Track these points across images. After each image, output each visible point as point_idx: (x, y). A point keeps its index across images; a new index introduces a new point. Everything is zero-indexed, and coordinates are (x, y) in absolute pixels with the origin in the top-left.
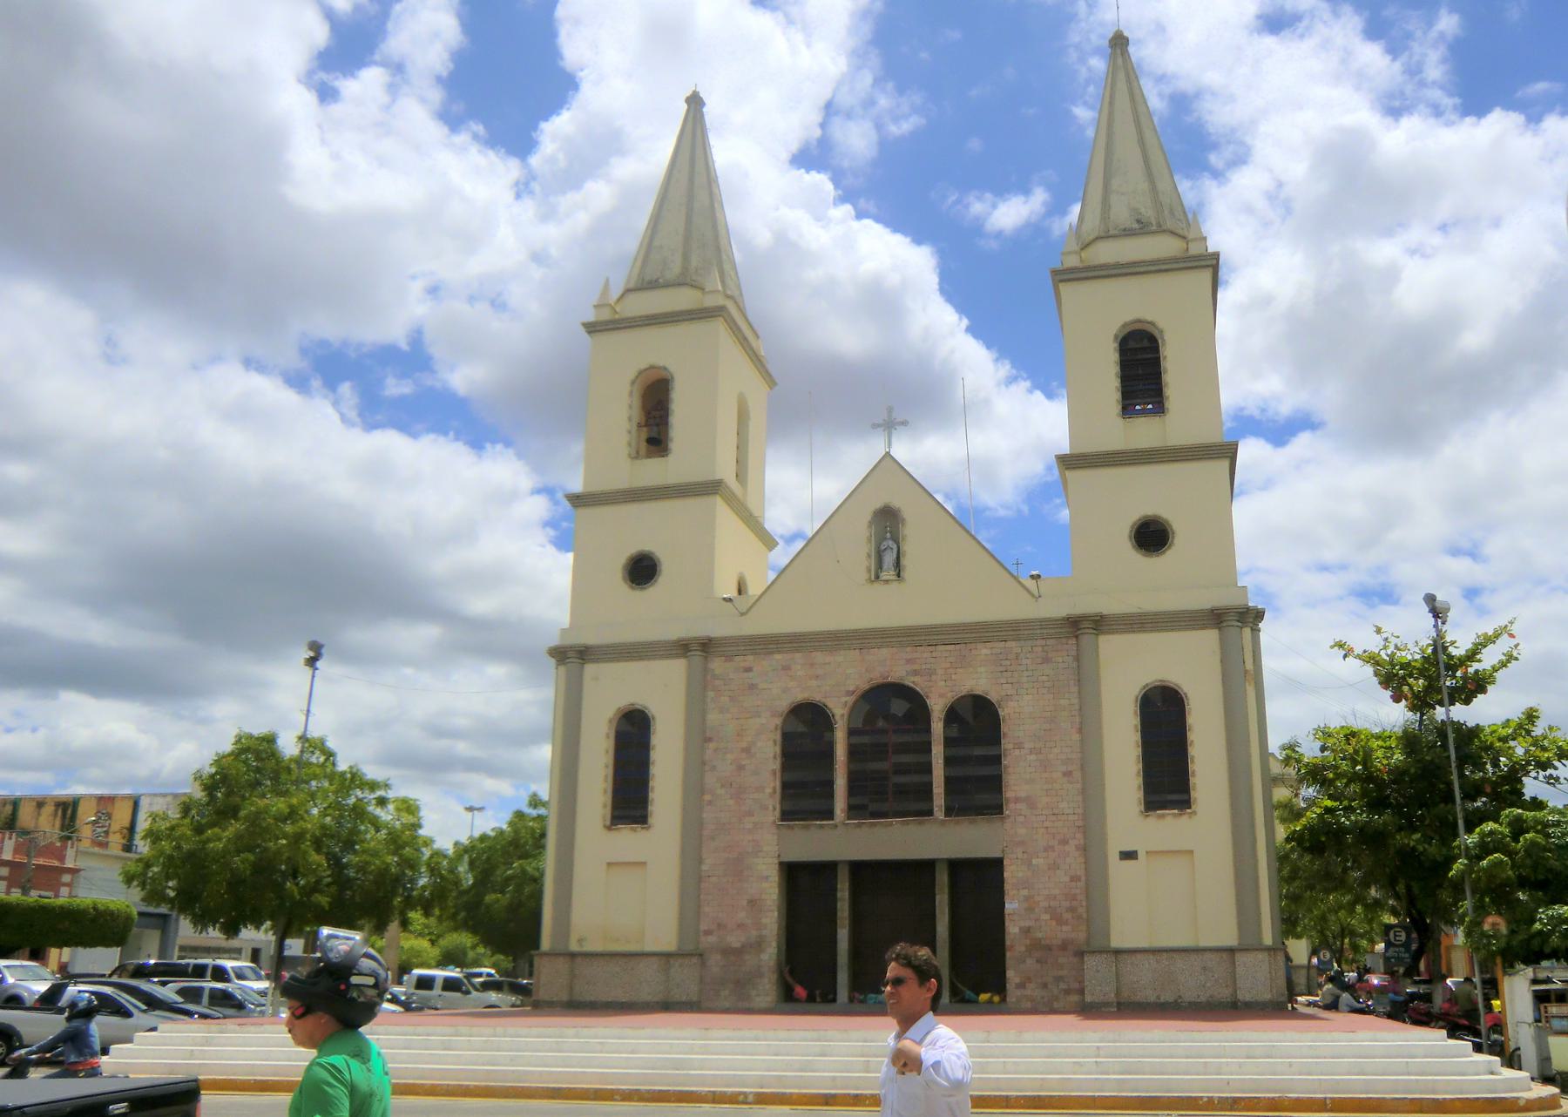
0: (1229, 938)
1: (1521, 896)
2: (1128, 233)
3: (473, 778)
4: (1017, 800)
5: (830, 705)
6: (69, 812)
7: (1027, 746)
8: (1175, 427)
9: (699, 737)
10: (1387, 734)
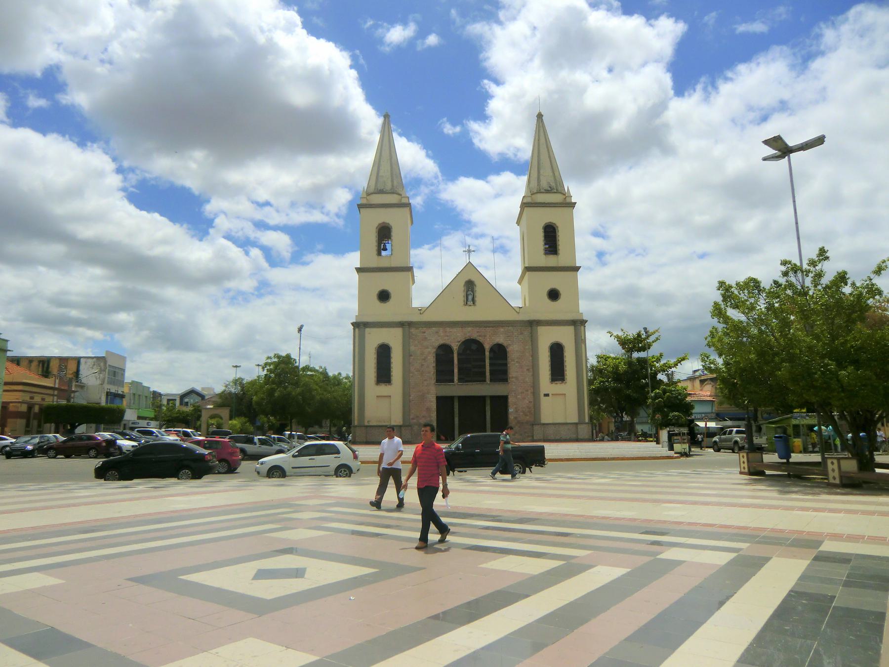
0: (576, 421)
1: (666, 410)
2: (547, 192)
3: (81, 330)
4: (512, 377)
5: (452, 345)
6: (46, 365)
7: (516, 361)
8: (561, 260)
9: (407, 356)
10: (617, 358)
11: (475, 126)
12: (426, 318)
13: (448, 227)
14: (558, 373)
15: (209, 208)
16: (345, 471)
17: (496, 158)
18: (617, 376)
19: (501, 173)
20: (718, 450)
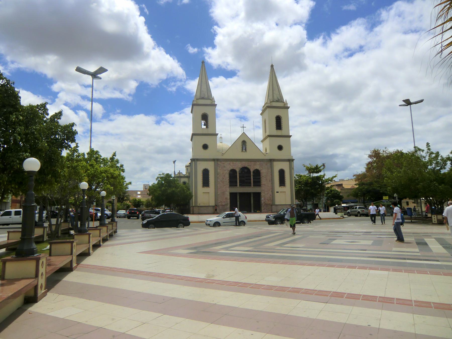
11: (209, 50)
12: (225, 157)
13: (188, 103)
14: (282, 183)
15: (55, 87)
16: (243, 223)
17: (215, 67)
18: (306, 183)
19: (219, 77)
20: (350, 216)
